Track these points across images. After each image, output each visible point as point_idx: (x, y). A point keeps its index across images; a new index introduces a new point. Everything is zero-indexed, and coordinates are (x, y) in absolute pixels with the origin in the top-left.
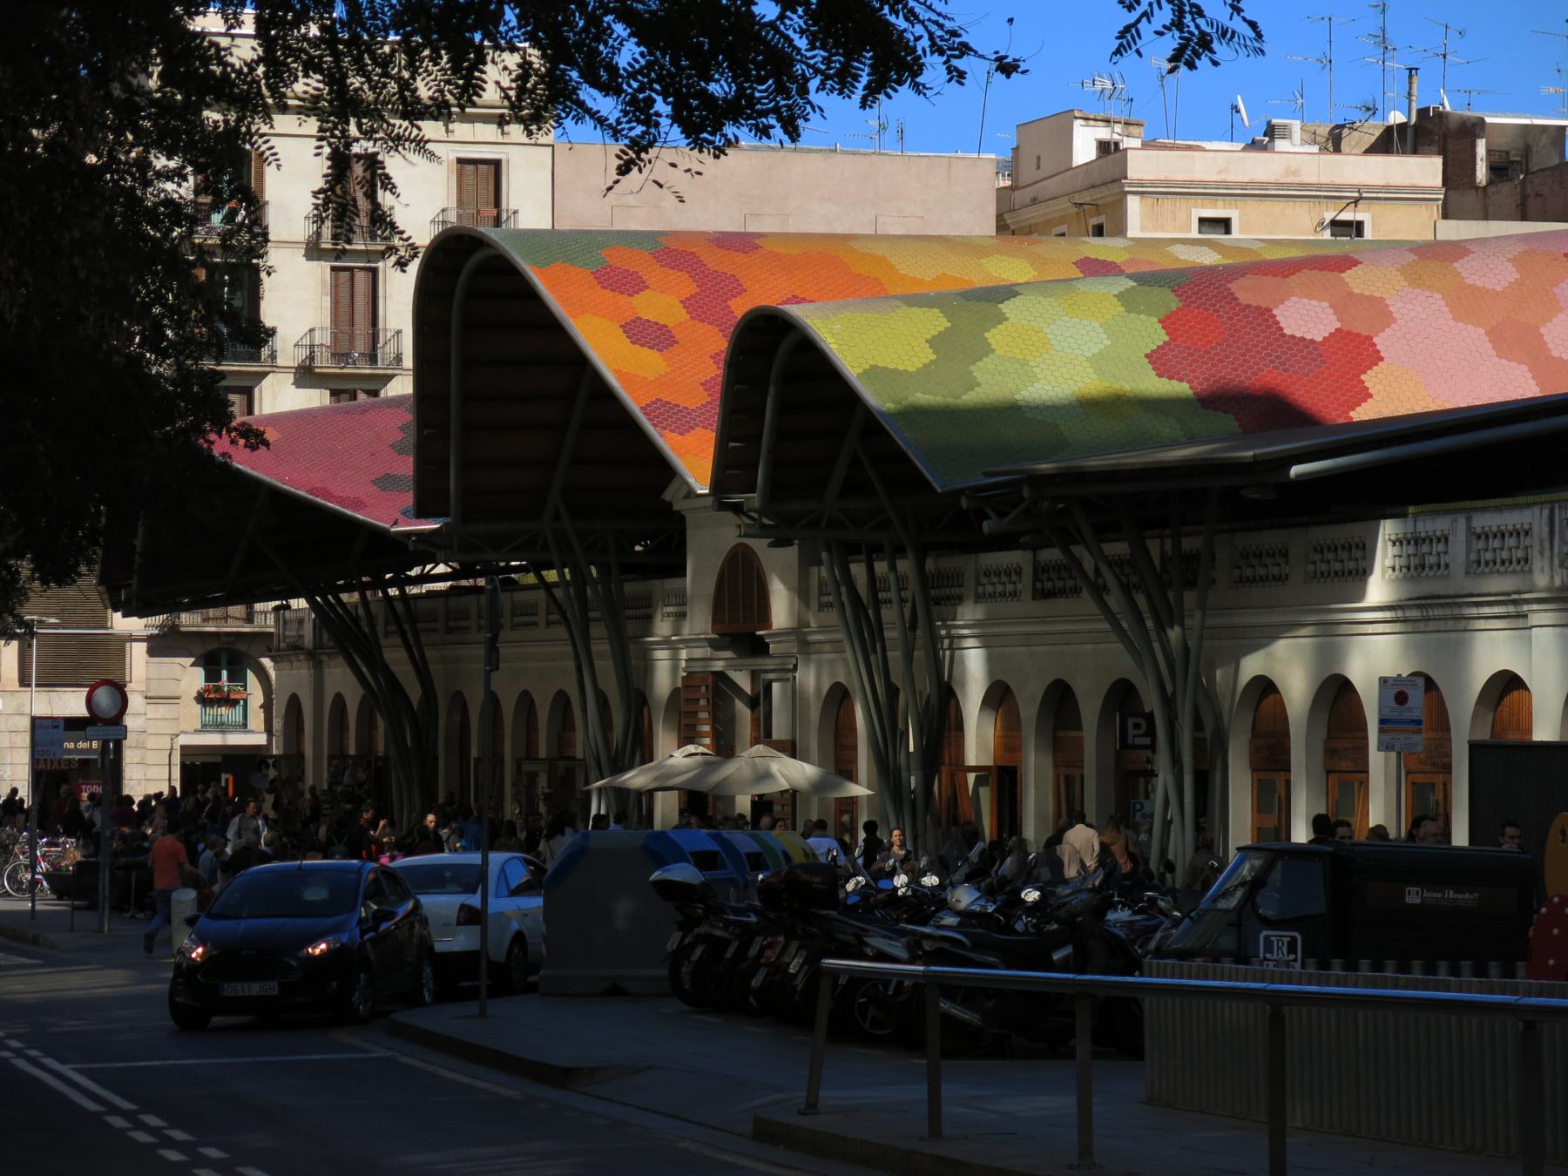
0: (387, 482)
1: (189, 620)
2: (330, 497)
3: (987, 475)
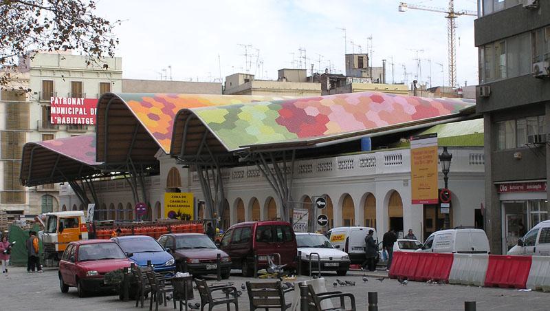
1: (39, 188)
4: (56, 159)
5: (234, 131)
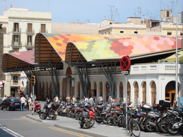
0: (31, 59)
2: (26, 61)
3: (92, 60)
4: (18, 61)
5: (91, 52)
